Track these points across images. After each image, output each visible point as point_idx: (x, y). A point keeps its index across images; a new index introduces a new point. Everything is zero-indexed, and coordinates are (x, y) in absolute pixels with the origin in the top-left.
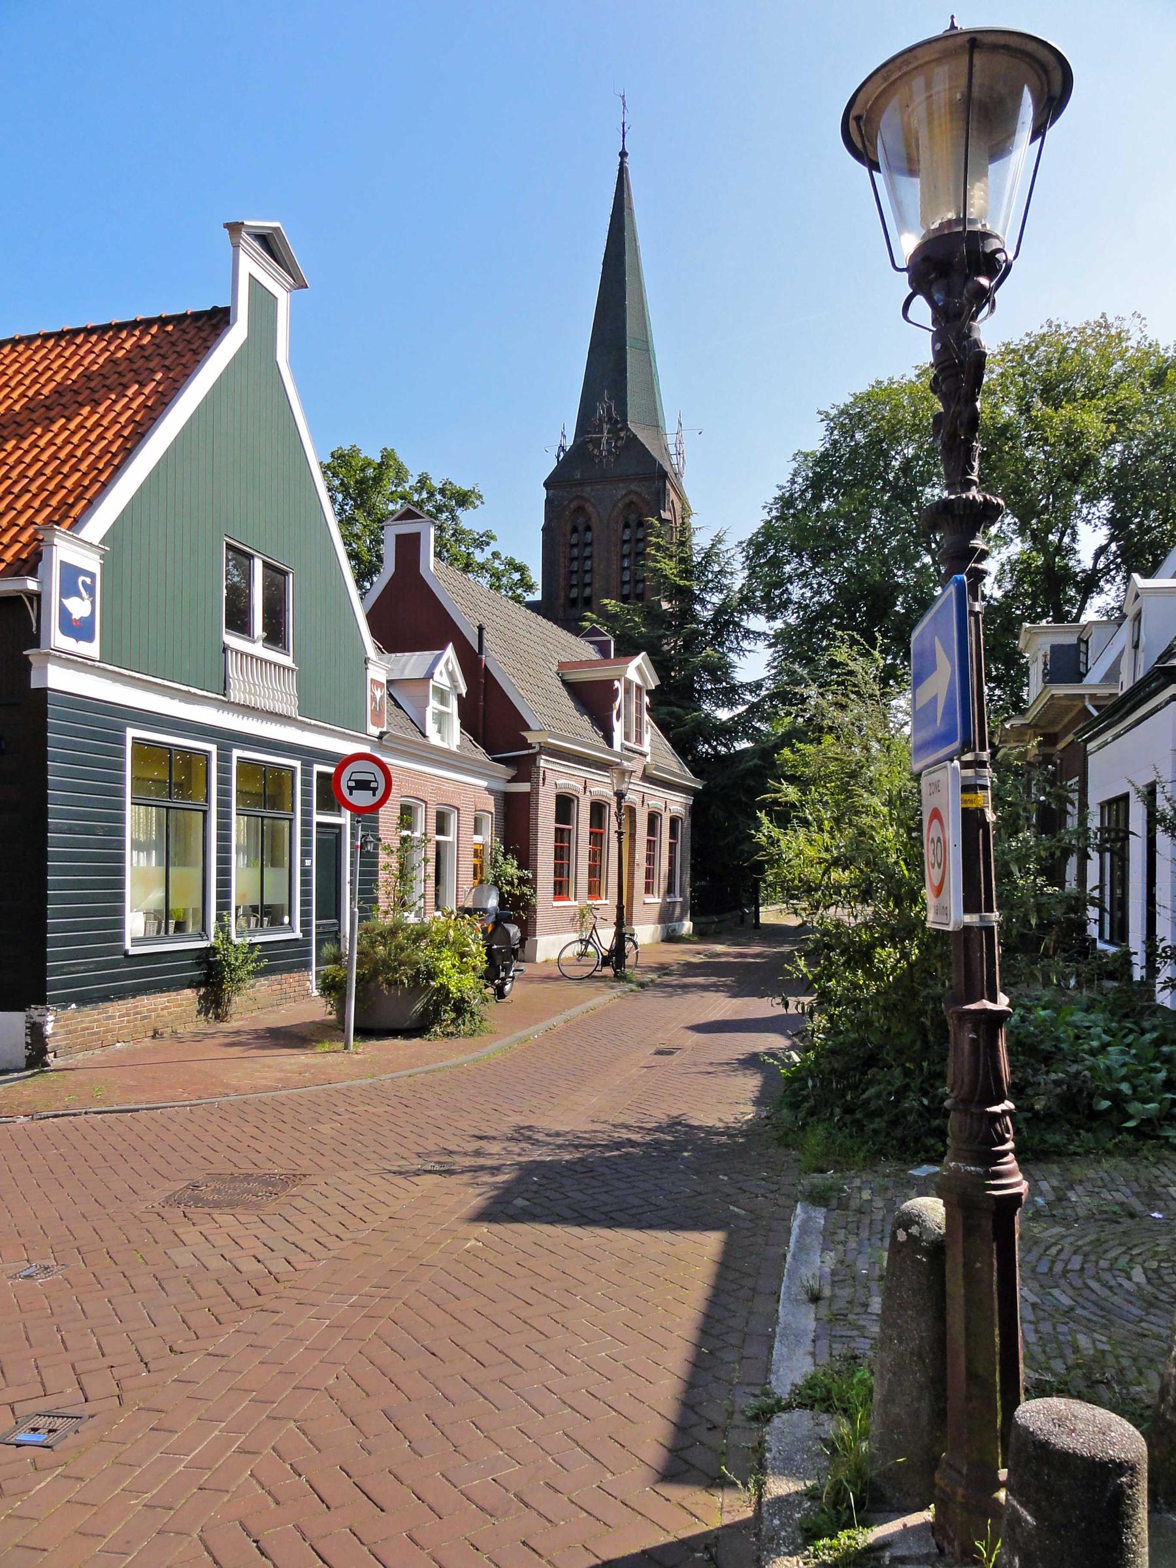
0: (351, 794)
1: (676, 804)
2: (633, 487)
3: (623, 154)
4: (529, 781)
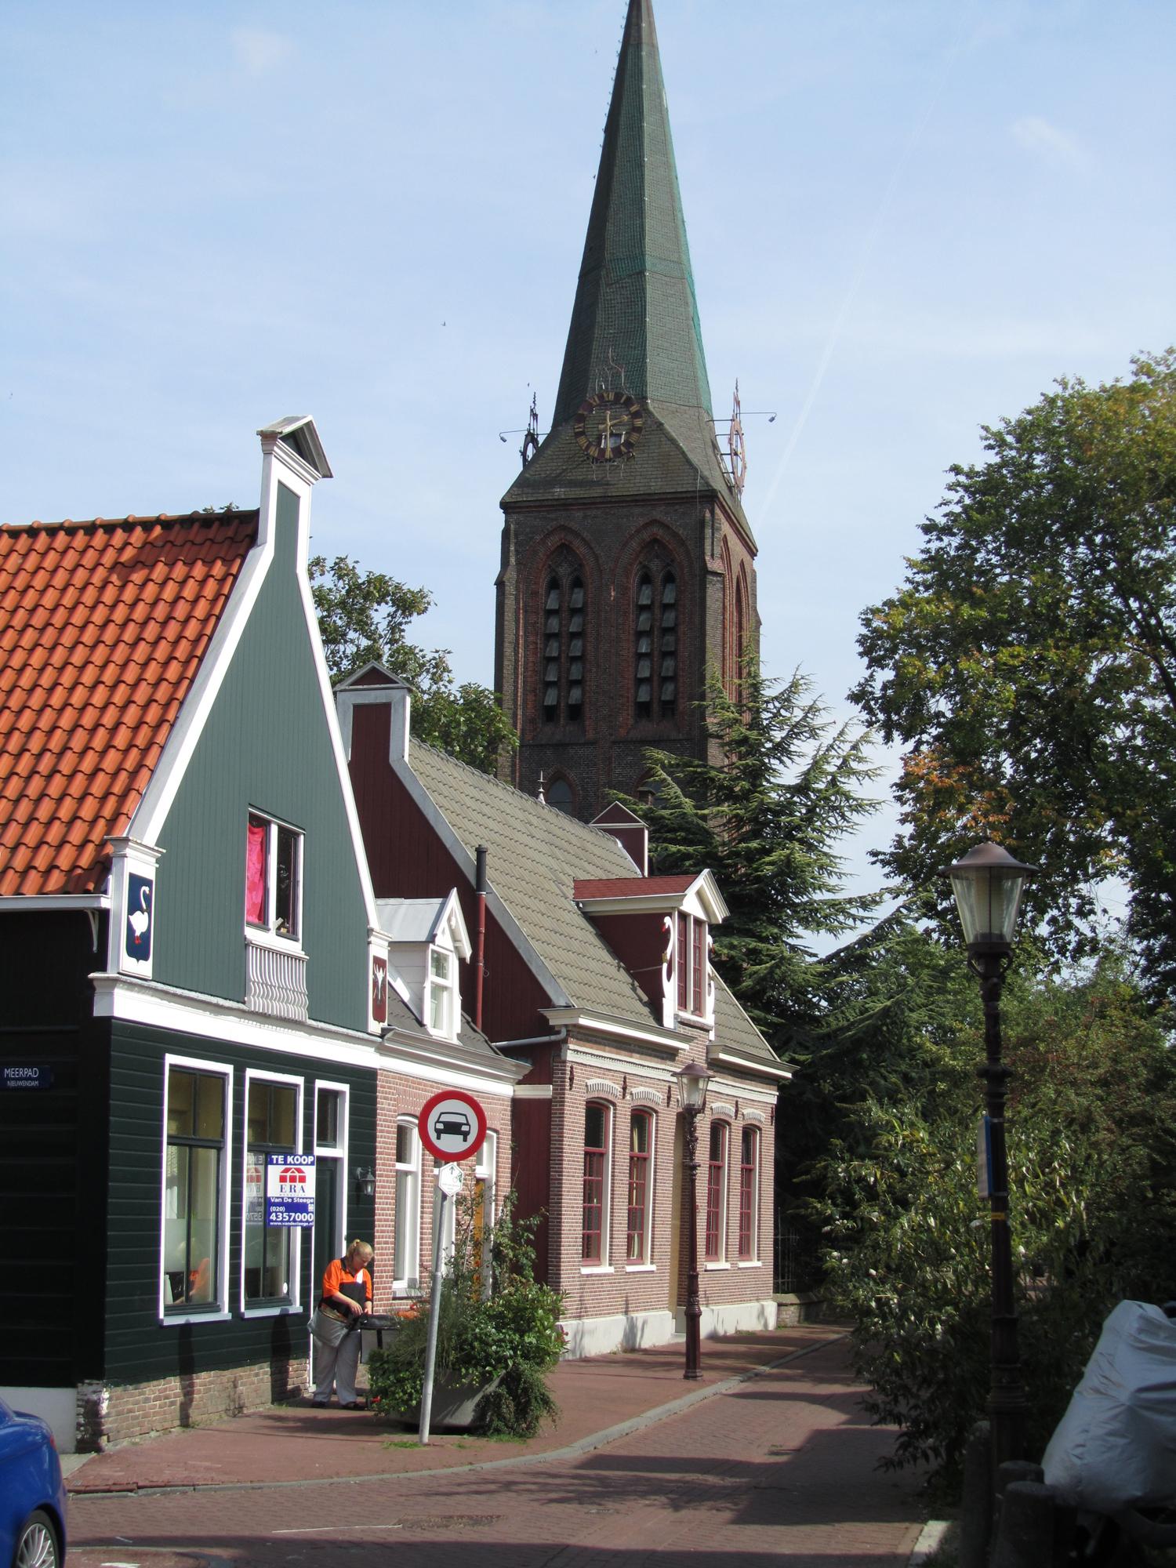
0: (439, 1138)
2: (658, 514)
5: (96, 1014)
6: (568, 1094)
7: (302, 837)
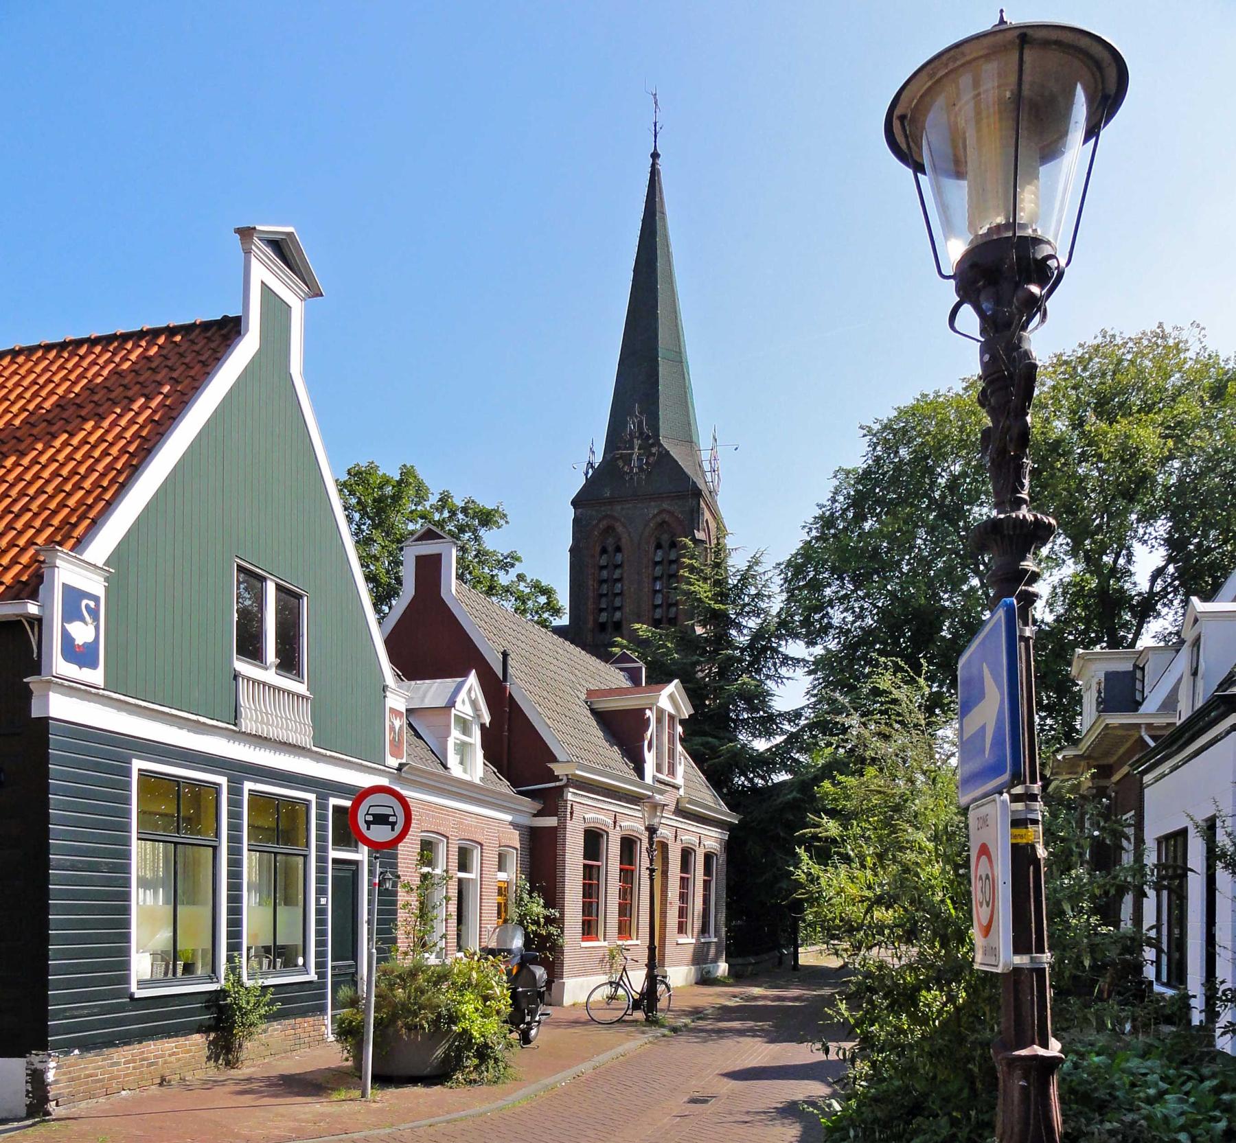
0: (368, 829)
1: (711, 839)
3: (655, 156)
4: (556, 815)
5: (33, 716)
6: (569, 824)
7: (305, 598)
